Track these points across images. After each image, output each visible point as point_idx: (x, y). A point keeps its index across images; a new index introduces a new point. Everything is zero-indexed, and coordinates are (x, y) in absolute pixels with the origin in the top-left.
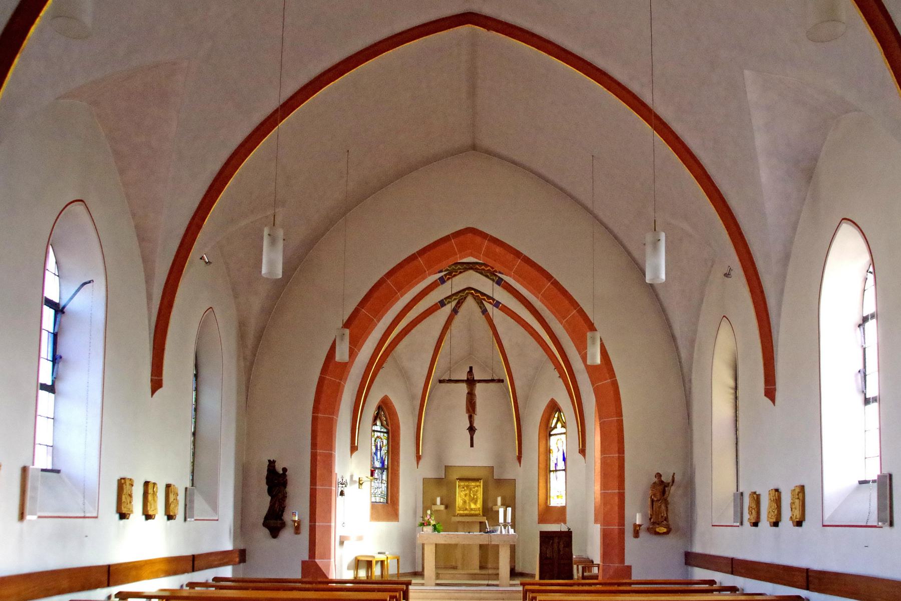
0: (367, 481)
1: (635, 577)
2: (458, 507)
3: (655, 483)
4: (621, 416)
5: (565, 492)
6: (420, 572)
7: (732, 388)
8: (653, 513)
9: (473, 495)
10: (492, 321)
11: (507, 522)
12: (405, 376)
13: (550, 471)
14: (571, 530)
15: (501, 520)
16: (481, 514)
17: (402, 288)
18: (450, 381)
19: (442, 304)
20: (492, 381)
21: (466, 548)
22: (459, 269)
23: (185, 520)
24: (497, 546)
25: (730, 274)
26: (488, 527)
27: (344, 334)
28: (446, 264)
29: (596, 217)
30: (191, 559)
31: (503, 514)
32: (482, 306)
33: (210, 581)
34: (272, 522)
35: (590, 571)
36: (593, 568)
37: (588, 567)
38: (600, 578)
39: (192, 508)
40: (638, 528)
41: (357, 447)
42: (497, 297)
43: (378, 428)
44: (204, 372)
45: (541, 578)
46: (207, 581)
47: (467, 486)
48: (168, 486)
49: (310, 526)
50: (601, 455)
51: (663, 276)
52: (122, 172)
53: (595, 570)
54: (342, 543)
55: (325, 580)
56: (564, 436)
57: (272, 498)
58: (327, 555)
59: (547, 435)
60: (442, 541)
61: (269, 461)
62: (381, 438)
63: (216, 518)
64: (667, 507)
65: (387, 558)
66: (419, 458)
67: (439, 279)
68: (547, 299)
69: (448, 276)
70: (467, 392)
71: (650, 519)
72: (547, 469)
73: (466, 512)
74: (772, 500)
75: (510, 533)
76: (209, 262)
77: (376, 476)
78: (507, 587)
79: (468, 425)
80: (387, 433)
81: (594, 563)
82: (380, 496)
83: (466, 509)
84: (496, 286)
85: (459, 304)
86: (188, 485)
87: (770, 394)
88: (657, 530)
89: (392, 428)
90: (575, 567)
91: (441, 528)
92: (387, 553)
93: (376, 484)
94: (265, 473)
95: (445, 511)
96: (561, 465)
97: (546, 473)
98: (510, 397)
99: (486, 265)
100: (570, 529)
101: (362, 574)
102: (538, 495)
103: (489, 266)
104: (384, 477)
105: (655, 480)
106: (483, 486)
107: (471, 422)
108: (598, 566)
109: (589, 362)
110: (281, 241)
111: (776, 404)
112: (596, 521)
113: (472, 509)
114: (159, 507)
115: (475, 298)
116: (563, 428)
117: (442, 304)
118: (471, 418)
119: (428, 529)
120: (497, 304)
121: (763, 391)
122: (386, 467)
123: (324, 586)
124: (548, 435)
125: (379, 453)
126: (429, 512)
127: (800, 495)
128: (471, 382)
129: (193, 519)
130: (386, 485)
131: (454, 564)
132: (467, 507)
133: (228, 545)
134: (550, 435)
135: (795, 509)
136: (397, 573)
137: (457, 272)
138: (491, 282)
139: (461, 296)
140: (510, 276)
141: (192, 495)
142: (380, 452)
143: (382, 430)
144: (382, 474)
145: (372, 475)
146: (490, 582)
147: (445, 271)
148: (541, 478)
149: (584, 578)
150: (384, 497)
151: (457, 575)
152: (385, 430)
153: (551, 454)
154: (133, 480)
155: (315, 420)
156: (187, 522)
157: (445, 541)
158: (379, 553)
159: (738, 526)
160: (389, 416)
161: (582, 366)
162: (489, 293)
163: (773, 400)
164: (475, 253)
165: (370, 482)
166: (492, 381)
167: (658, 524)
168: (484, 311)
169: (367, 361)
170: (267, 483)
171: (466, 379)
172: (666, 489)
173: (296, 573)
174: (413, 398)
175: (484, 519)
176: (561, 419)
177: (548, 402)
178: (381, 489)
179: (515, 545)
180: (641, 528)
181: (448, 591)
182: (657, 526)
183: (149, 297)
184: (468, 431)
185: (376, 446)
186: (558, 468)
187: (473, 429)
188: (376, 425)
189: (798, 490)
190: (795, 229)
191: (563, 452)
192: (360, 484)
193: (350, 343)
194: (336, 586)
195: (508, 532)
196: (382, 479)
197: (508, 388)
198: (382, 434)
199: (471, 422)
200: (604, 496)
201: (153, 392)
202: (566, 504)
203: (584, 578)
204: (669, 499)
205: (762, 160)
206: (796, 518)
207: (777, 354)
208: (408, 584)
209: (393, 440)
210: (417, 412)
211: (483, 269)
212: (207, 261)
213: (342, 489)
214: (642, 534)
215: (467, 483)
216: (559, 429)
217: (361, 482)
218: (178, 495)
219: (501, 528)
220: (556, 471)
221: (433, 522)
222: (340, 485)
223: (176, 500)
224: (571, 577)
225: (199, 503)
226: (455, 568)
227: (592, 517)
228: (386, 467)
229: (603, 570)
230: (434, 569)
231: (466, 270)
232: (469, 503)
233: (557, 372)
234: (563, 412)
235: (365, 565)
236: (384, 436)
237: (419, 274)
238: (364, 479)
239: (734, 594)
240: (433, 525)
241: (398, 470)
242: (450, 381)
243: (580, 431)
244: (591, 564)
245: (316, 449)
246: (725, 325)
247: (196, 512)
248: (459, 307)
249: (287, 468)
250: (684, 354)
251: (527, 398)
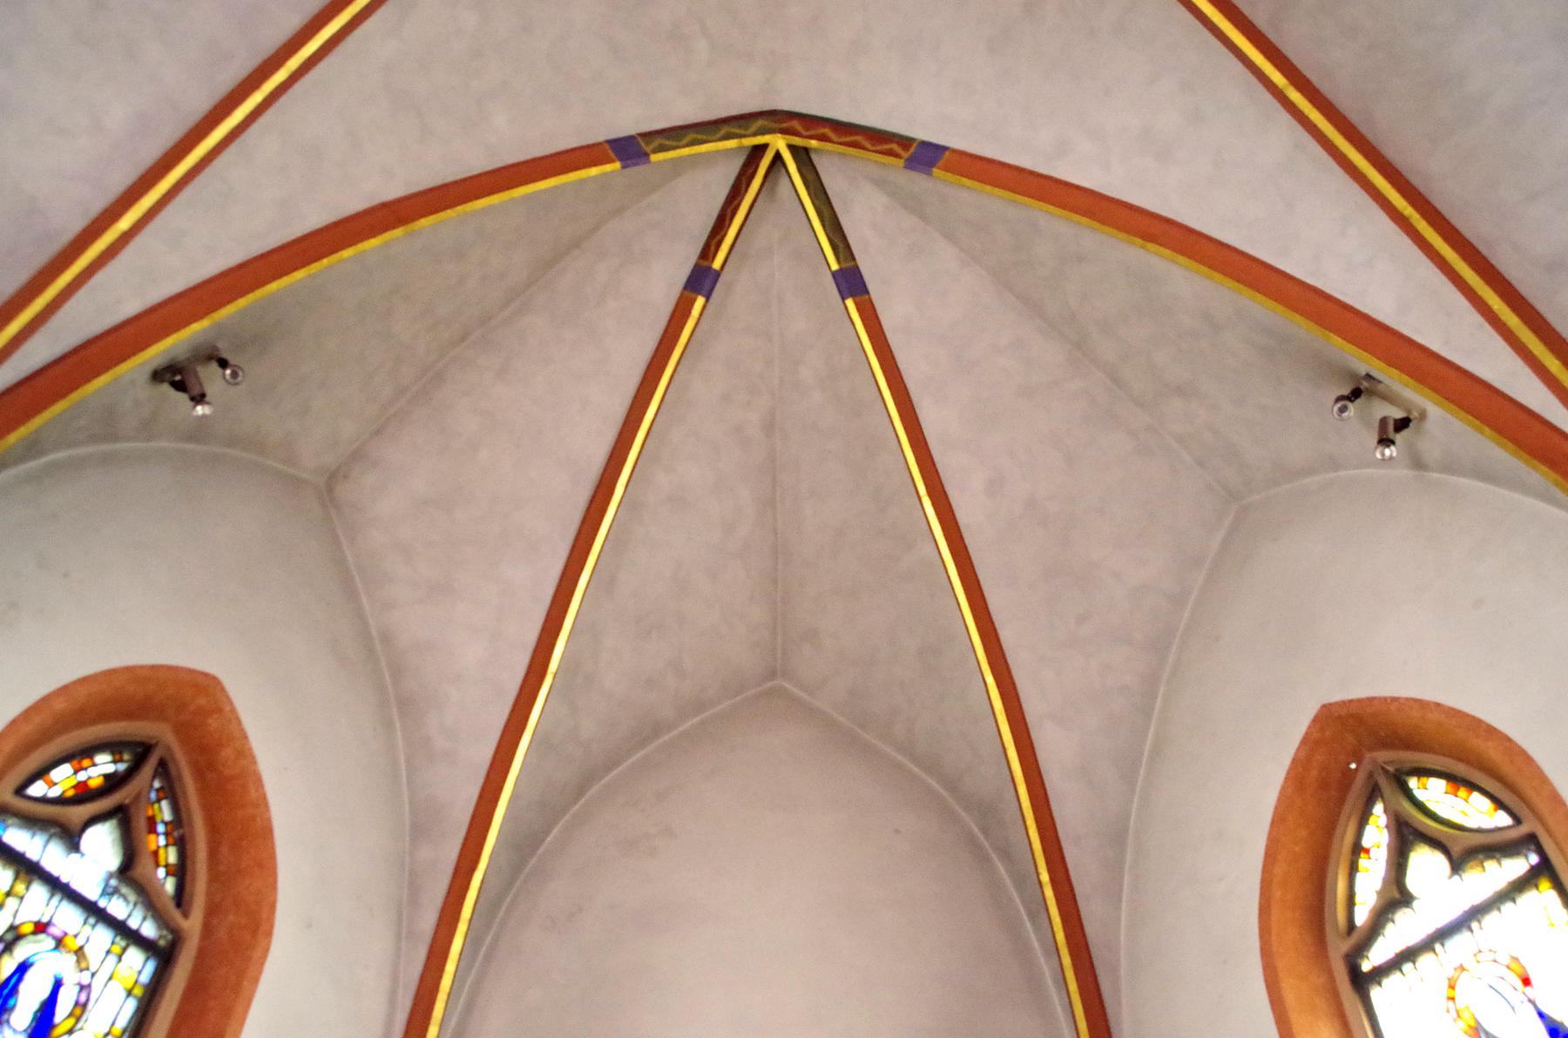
80: (164, 955)
89: (208, 929)
134: (1362, 982)
143: (117, 908)
174: (420, 828)
210: (428, 921)
251: (1117, 836)
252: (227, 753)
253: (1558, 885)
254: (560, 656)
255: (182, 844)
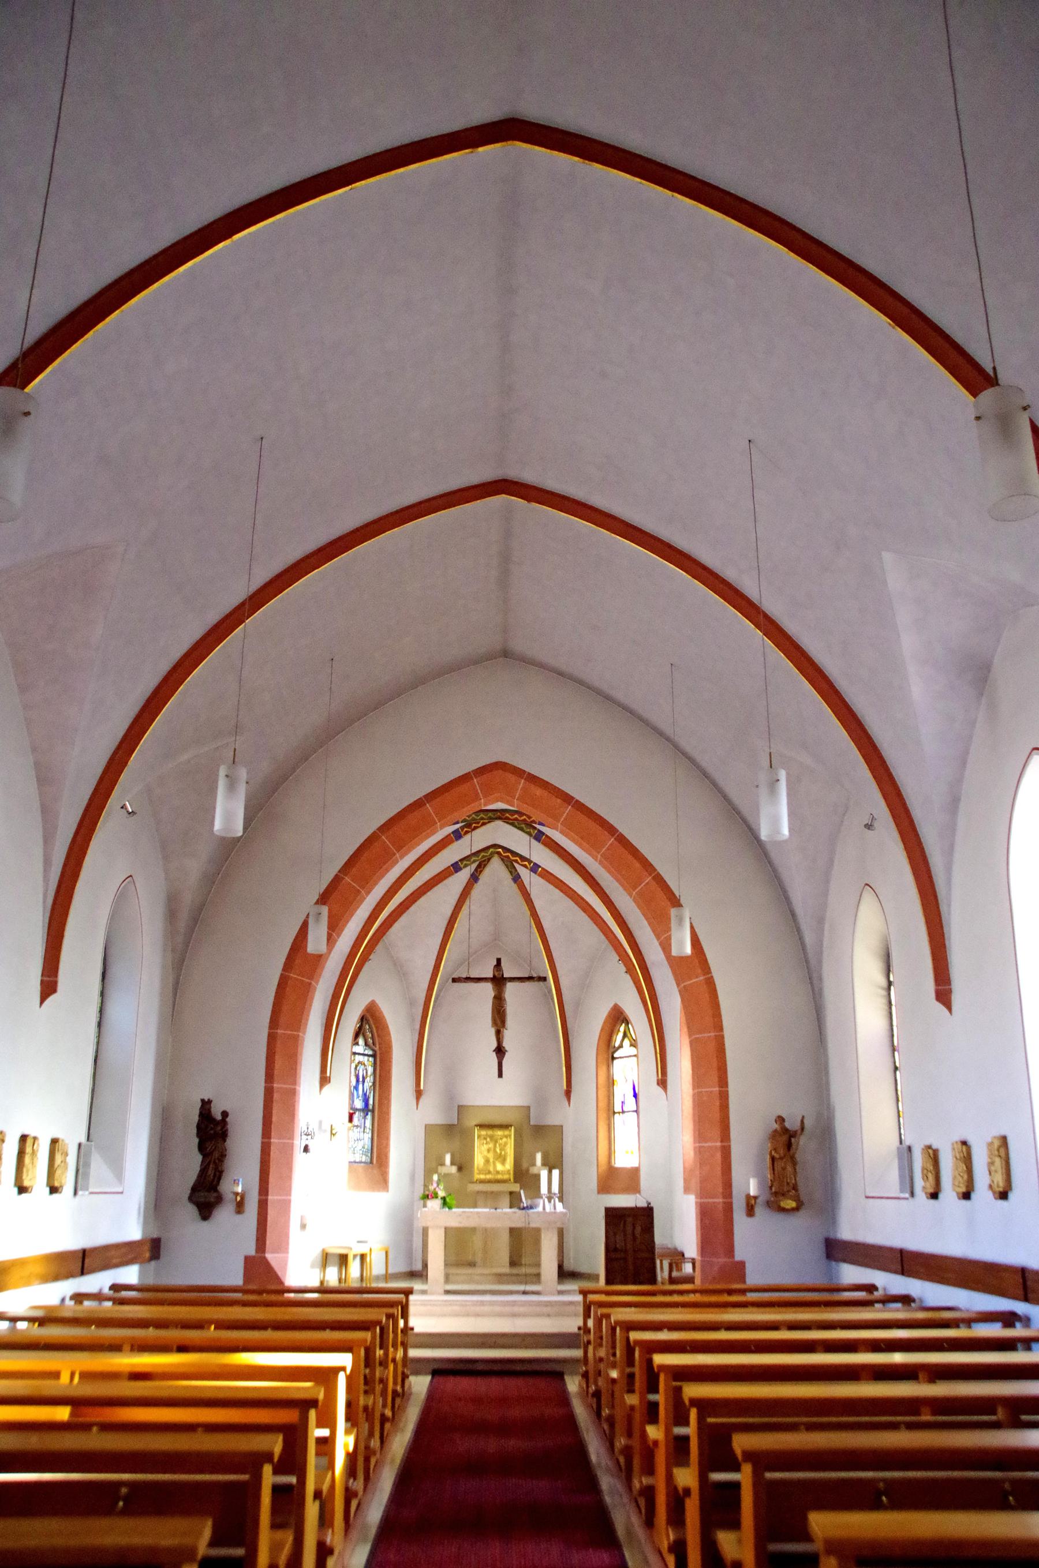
1: (753, 1278)
2: (478, 1168)
3: (775, 1131)
4: (721, 1029)
6: (419, 1272)
7: (883, 989)
8: (774, 1178)
9: (500, 1150)
10: (529, 895)
11: (553, 1192)
12: (400, 971)
15: (544, 1189)
16: (512, 1180)
17: (402, 845)
18: (468, 979)
19: (456, 867)
20: (530, 979)
21: (488, 1234)
22: (482, 819)
23: (75, 1193)
24: (538, 1231)
25: (873, 826)
27: (320, 914)
28: (466, 812)
29: (676, 747)
30: (81, 1255)
31: (548, 1180)
32: (513, 870)
33: (106, 1290)
34: (202, 1196)
35: (679, 1269)
36: (683, 1265)
38: (698, 1281)
39: (87, 1175)
40: (753, 1202)
41: (330, 1078)
42: (535, 859)
43: (360, 1048)
44: (114, 971)
45: (609, 1281)
46: (101, 1290)
48: (54, 1142)
49: (260, 1201)
51: (785, 831)
52: (23, 689)
53: (688, 1268)
55: (279, 1287)
57: (203, 1158)
58: (283, 1246)
60: (454, 1223)
61: (203, 1101)
62: (364, 1064)
63: (120, 1190)
64: (795, 1169)
66: (419, 1094)
67: (453, 832)
68: (610, 862)
69: (465, 829)
70: (493, 995)
71: (771, 1188)
72: (609, 1110)
73: (489, 1177)
74: (958, 1157)
76: (133, 812)
79: (495, 1045)
80: (374, 1056)
81: (686, 1256)
83: (489, 1172)
84: (534, 842)
85: (481, 867)
86: (83, 1139)
87: (944, 996)
88: (782, 1204)
90: (658, 1262)
93: (356, 1133)
94: (196, 1118)
95: (458, 1175)
97: (609, 1114)
98: (553, 1002)
99: (521, 814)
100: (650, 1204)
101: (332, 1278)
103: (524, 814)
105: (776, 1126)
106: (515, 1135)
108: (693, 1262)
109: (674, 952)
110: (244, 784)
111: (954, 1008)
112: (687, 1190)
113: (498, 1172)
114: (37, 1175)
115: (503, 859)
117: (456, 867)
118: (499, 1034)
119: (434, 1204)
120: (535, 868)
121: (933, 995)
122: (371, 1107)
123: (273, 1298)
124: (610, 1059)
125: (361, 1086)
126: (435, 1177)
127: (1000, 1151)
128: (499, 981)
129: (87, 1193)
130: (370, 1135)
132: (491, 1169)
133: (133, 1232)
134: (613, 1058)
135: (996, 1171)
138: (527, 837)
140: (556, 829)
141: (88, 1155)
142: (363, 1085)
144: (365, 1118)
145: (351, 1120)
146: (529, 1288)
147: (462, 822)
149: (672, 1281)
150: (367, 1154)
154: (5, 1134)
155: (272, 1038)
156: (78, 1197)
157: (460, 1223)
159: (907, 1199)
160: (377, 1031)
161: (662, 956)
162: (525, 853)
163: (948, 1005)
164: (508, 794)
166: (530, 979)
167: (783, 1195)
168: (517, 878)
170: (198, 1135)
171: (492, 976)
172: (793, 1140)
173: (235, 1278)
174: (412, 1003)
175: (516, 1187)
176: (629, 1035)
177: (609, 1009)
178: (362, 1141)
179: (563, 1228)
180: (758, 1201)
182: (781, 1198)
183: (47, 862)
184: (495, 1053)
187: (502, 1051)
188: (357, 1044)
189: (997, 1143)
190: (964, 763)
192: (332, 1134)
193: (329, 928)
197: (551, 990)
200: (699, 1151)
201: (43, 1000)
202: (639, 1165)
203: (672, 1281)
204: (798, 1157)
205: (912, 669)
206: (998, 1186)
207: (949, 940)
208: (408, 1292)
210: (418, 1026)
212: (130, 810)
214: (759, 1210)
215: (490, 1132)
216: (627, 1049)
218: (67, 1155)
219: (554, 1201)
220: (623, 1112)
221: (441, 1193)
222: (304, 1137)
223: (65, 1162)
224: (653, 1280)
225: (98, 1166)
226: (472, 1264)
227: (680, 1183)
228: (371, 1107)
229: (703, 1270)
230: (442, 1267)
231: (491, 820)
233: (622, 965)
235: (337, 1260)
236: (368, 1061)
237: (426, 826)
239: (906, 1308)
240: (441, 1198)
242: (468, 979)
244: (681, 1258)
245: (272, 1082)
246: (868, 897)
247: (92, 1180)
248: (481, 872)
249: (228, 1111)
250: (809, 938)
251: (578, 1004)
252: (377, 1013)
253: (638, 1059)
254: (398, 875)
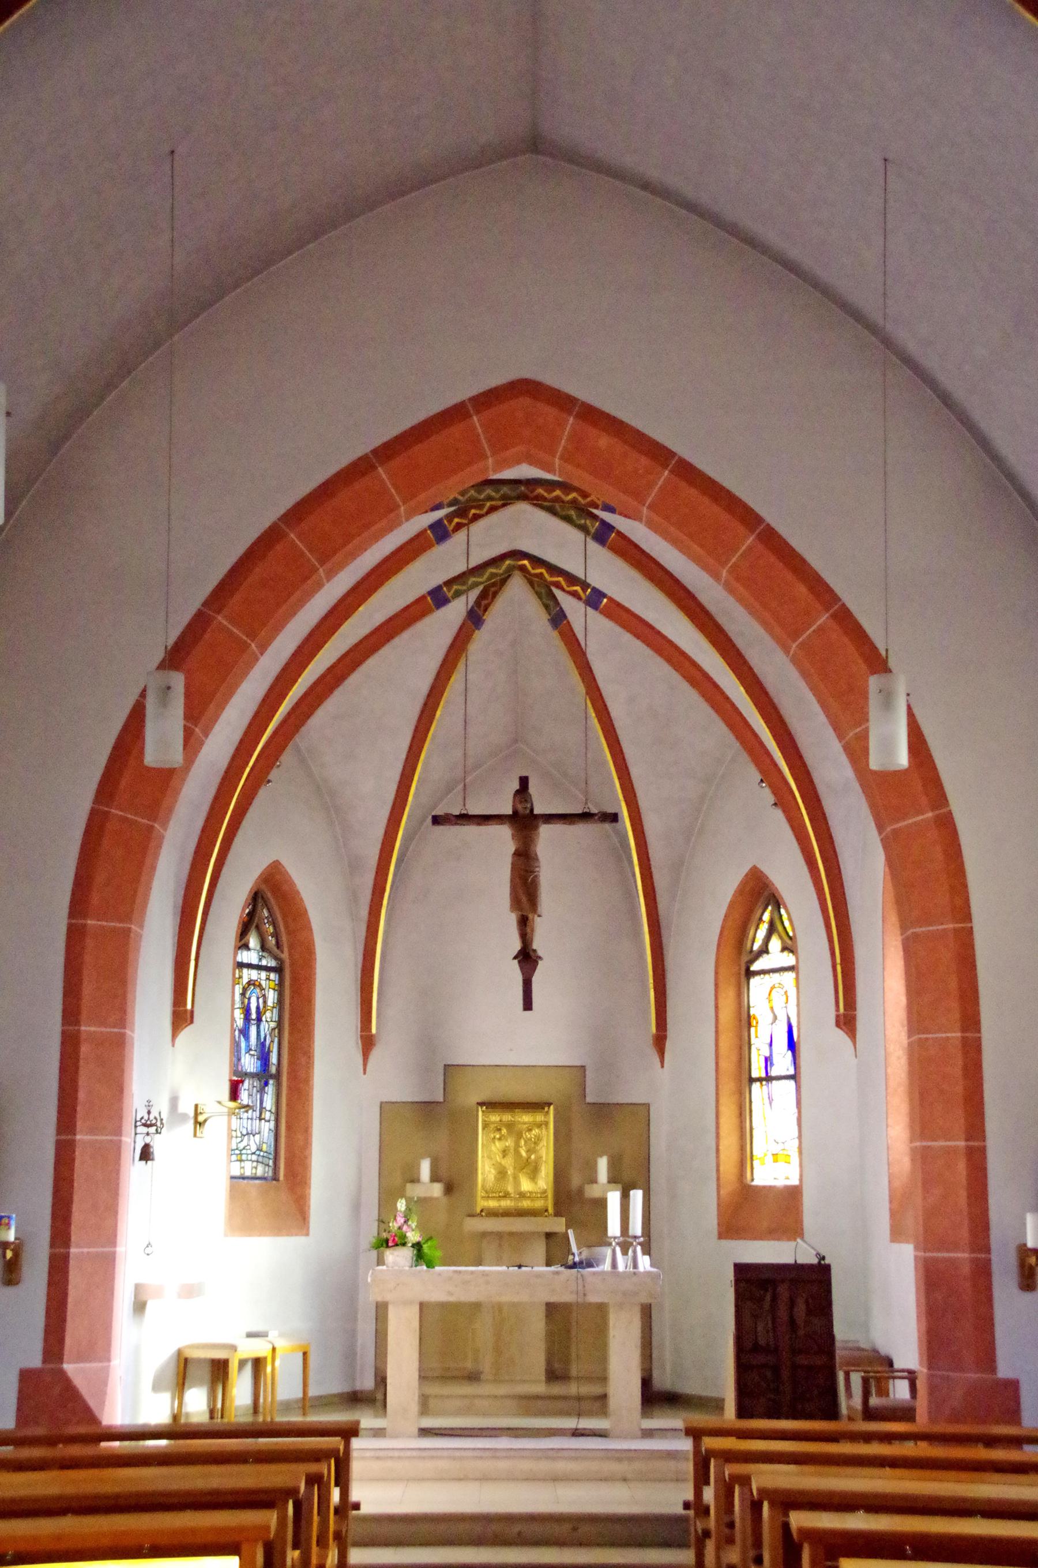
0: (221, 1114)
2: (483, 1186)
4: (968, 917)
5: (797, 1142)
9: (528, 1151)
11: (631, 1233)
13: (752, 1080)
14: (827, 1261)
15: (614, 1228)
16: (551, 1210)
18: (464, 818)
19: (438, 597)
20: (585, 816)
22: (490, 498)
24: (602, 1309)
26: (574, 1248)
27: (169, 688)
28: (453, 487)
32: (551, 603)
35: (883, 1392)
37: (878, 1380)
41: (192, 1012)
42: (596, 580)
45: (743, 1412)
47: (510, 1126)
50: (911, 1033)
53: (901, 1391)
54: (140, 1307)
56: (791, 975)
59: (739, 974)
60: (437, 1295)
62: (260, 985)
65: (274, 1349)
66: (368, 1043)
67: (432, 527)
73: (506, 1204)
75: (641, 1269)
77: (244, 1097)
78: (634, 1437)
79: (517, 946)
80: (279, 970)
82: (254, 1157)
83: (506, 1196)
84: (593, 546)
85: (488, 597)
89: (290, 954)
91: (438, 1254)
92: (273, 1335)
93: (245, 1122)
95: (444, 1200)
96: (783, 1063)
98: (631, 862)
100: (823, 1258)
102: (718, 1150)
104: (269, 1102)
106: (555, 1122)
107: (526, 937)
108: (911, 1377)
109: (875, 763)
112: (897, 1234)
113: (522, 1195)
115: (531, 580)
116: (786, 953)
117: (438, 597)
118: (524, 924)
119: (399, 1258)
120: (595, 599)
124: (743, 972)
125: (253, 1030)
126: (401, 1205)
130: (272, 1124)
131: (469, 1365)
132: (510, 1189)
134: (749, 974)
136: (301, 1395)
137: (480, 507)
138: (578, 536)
139: (493, 575)
143: (264, 963)
144: (262, 1091)
145: (234, 1095)
147: (450, 505)
148: (723, 1100)
150: (266, 1160)
151: (477, 1402)
152: (272, 963)
153: (753, 1030)
155: (75, 936)
157: (450, 1293)
158: (250, 1335)
162: (575, 567)
165: (226, 1118)
166: (585, 816)
168: (558, 619)
169: (223, 762)
171: (511, 813)
174: (354, 866)
175: (558, 1225)
176: (780, 928)
178: (257, 1137)
181: (458, 1454)
184: (516, 961)
185: (247, 1011)
186: (774, 1072)
188: (246, 947)
191: (789, 1019)
192: (199, 1124)
194: (120, 1447)
195: (635, 1266)
196: (262, 1108)
198: (264, 974)
199: (526, 937)
200: (923, 1158)
202: (801, 1180)
203: (869, 1414)
209: (296, 992)
210: (364, 913)
211: (557, 499)
213: (148, 1140)
215: (507, 1117)
216: (776, 957)
217: (201, 1119)
220: (768, 1078)
221: (413, 1237)
222: (142, 1130)
224: (831, 1412)
226: (473, 1377)
229: (932, 1389)
231: (507, 501)
232: (516, 1178)
234: (786, 908)
235: (206, 1372)
238: (209, 1108)
240: (413, 1246)
241: (308, 1080)
242: (464, 818)
243: (838, 960)
245: (77, 1023)
251: (678, 866)
255: (274, 924)
